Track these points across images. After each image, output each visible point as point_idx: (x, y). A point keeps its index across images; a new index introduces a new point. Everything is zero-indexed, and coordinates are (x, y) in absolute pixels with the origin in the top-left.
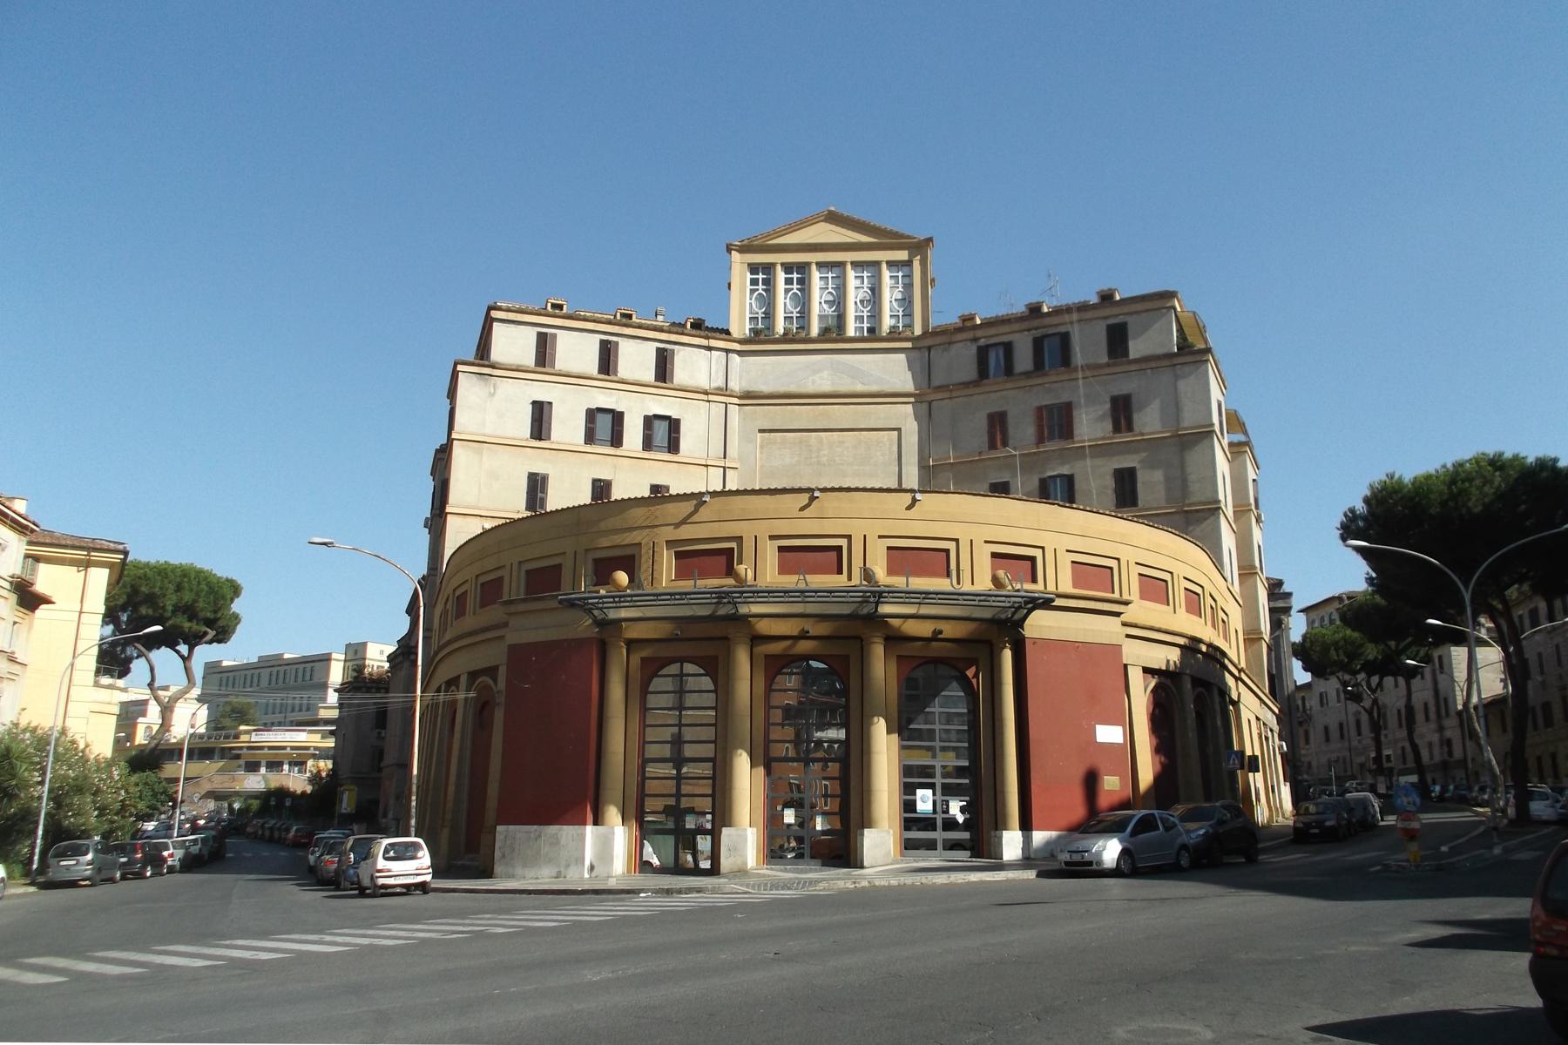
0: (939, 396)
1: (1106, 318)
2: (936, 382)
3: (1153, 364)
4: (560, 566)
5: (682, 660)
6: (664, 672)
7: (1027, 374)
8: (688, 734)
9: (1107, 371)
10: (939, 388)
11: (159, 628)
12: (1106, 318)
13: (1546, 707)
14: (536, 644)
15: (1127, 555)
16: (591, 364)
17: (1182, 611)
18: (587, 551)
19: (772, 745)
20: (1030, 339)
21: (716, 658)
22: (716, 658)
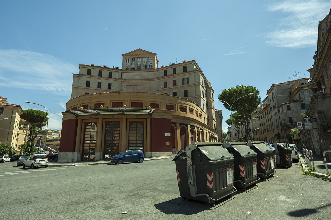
0: (157, 79)
1: (183, 65)
2: (156, 77)
3: (191, 73)
4: (77, 107)
5: (92, 123)
6: (89, 125)
7: (185, 79)
8: (315, 167)
9: (183, 74)
10: (157, 78)
11: (7, 118)
12: (183, 65)
13: (90, 101)
14: (67, 120)
15: (195, 109)
16: (107, 76)
17: (195, 116)
18: (81, 104)
19: (130, 141)
20: (172, 69)
21: (97, 122)
22: (97, 122)
